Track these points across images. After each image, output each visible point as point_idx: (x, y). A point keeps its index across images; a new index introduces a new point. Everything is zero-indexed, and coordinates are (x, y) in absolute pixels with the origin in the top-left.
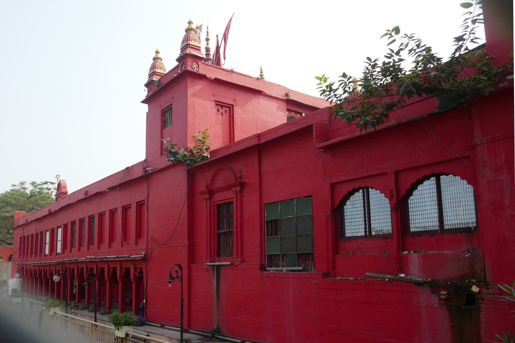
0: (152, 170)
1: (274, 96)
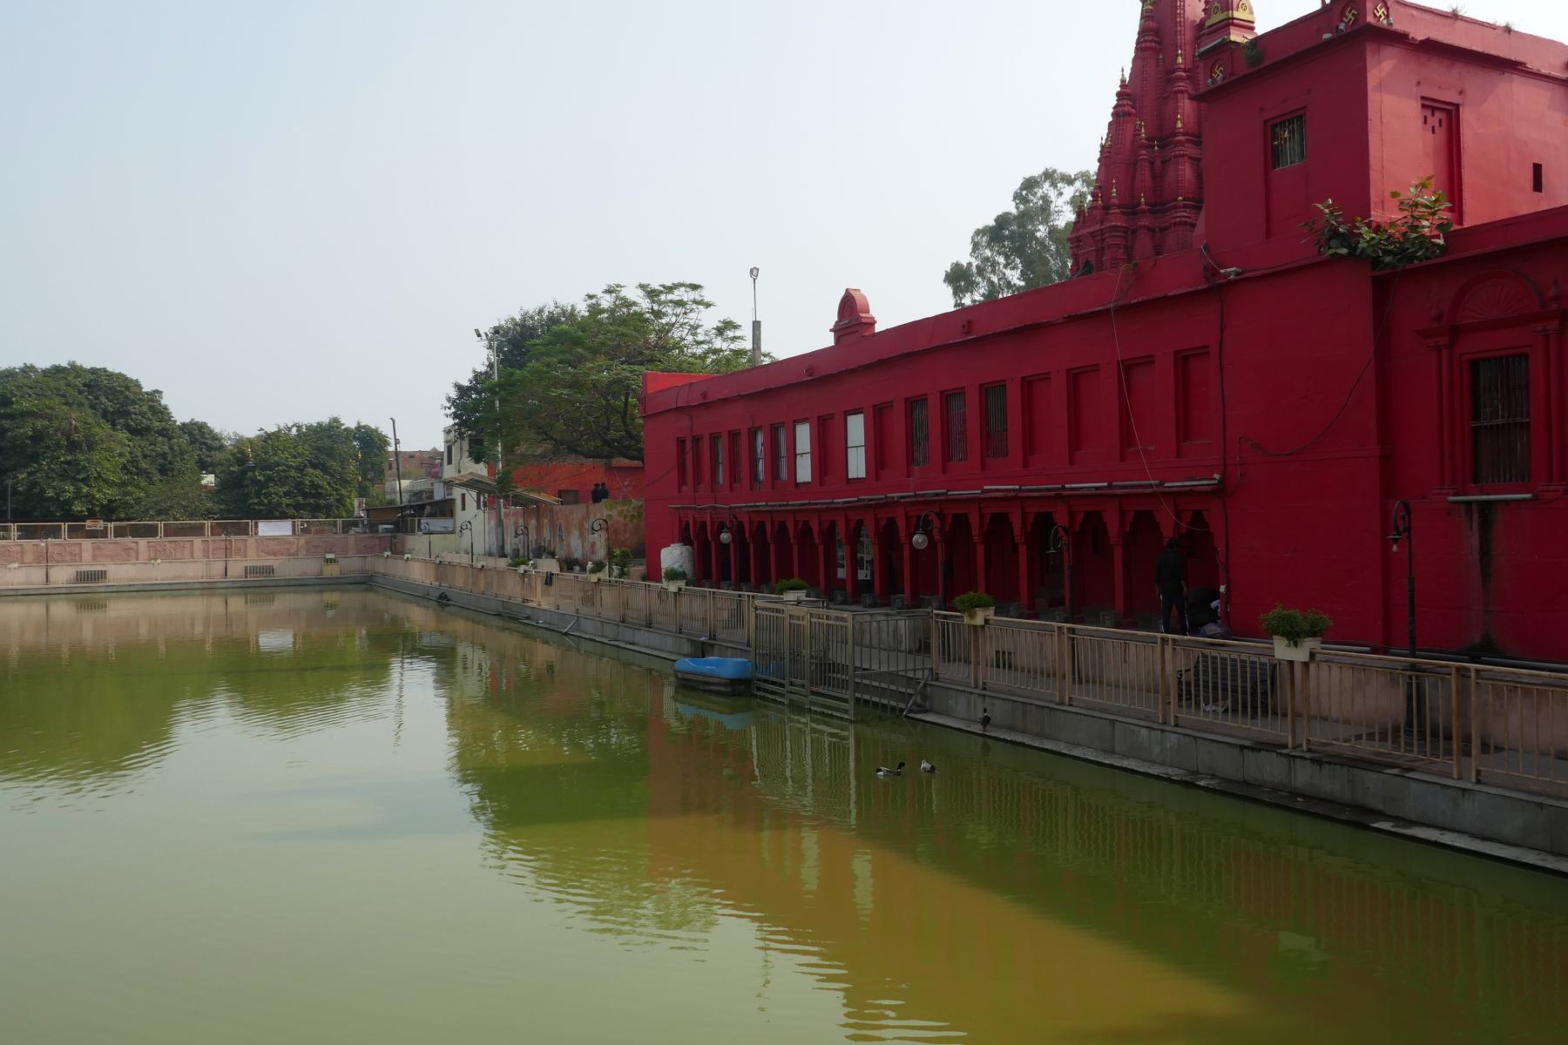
0: (1237, 274)
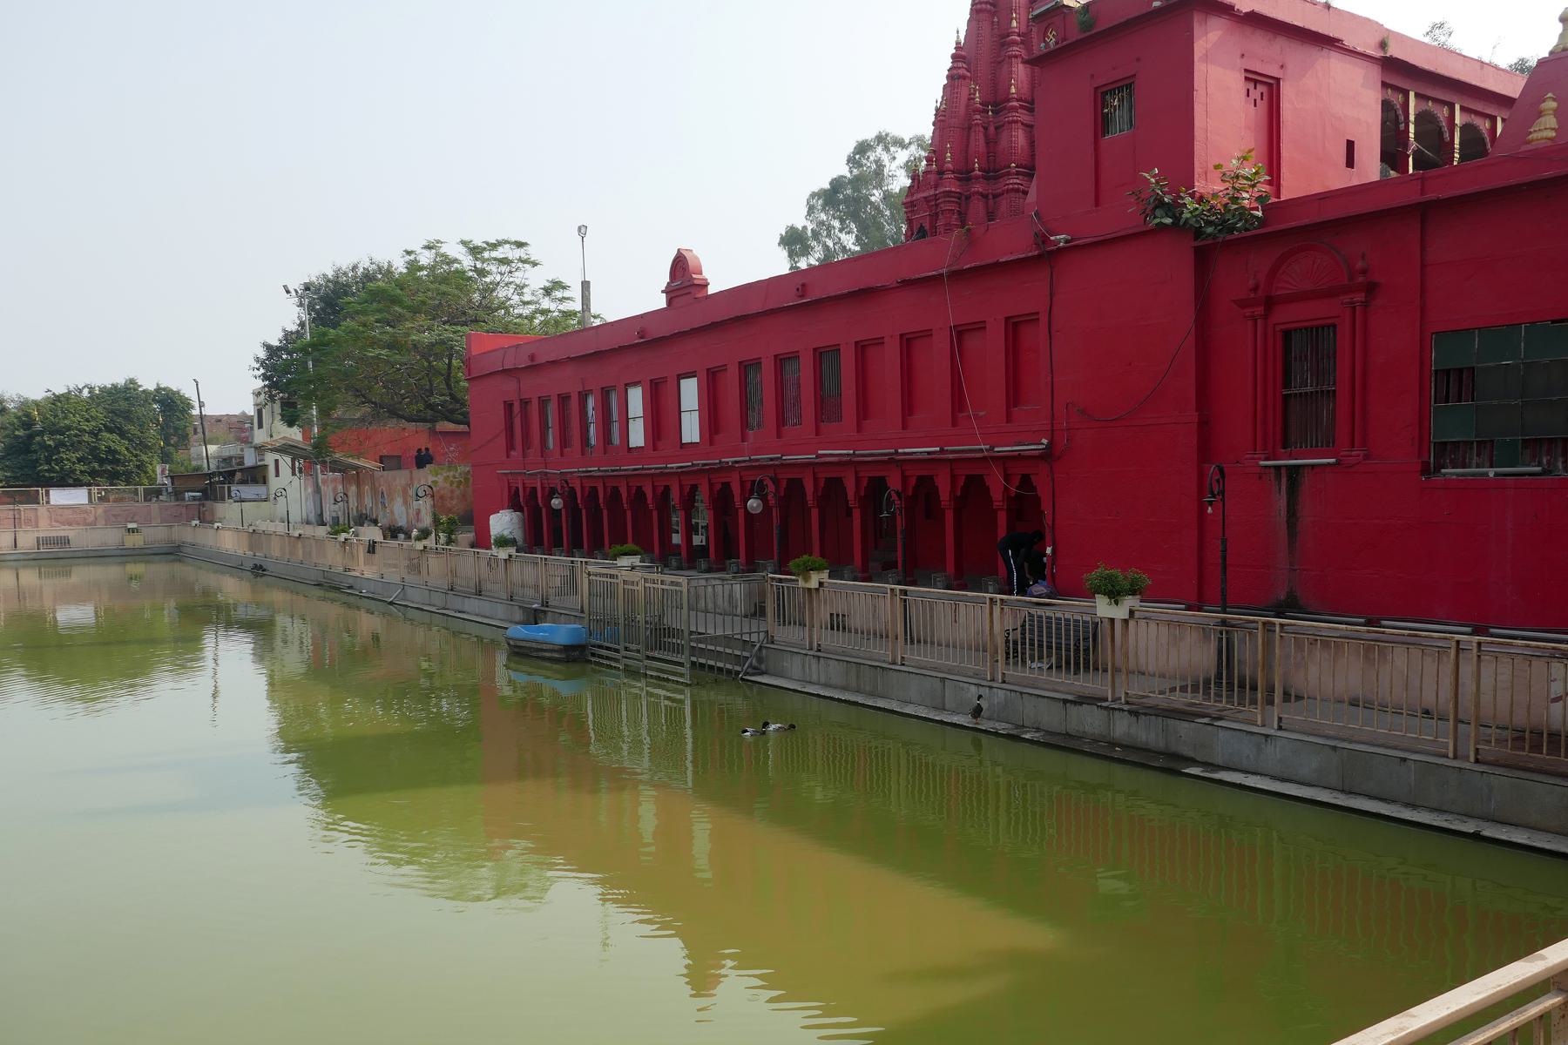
0: (1067, 241)
1: (1359, 49)
